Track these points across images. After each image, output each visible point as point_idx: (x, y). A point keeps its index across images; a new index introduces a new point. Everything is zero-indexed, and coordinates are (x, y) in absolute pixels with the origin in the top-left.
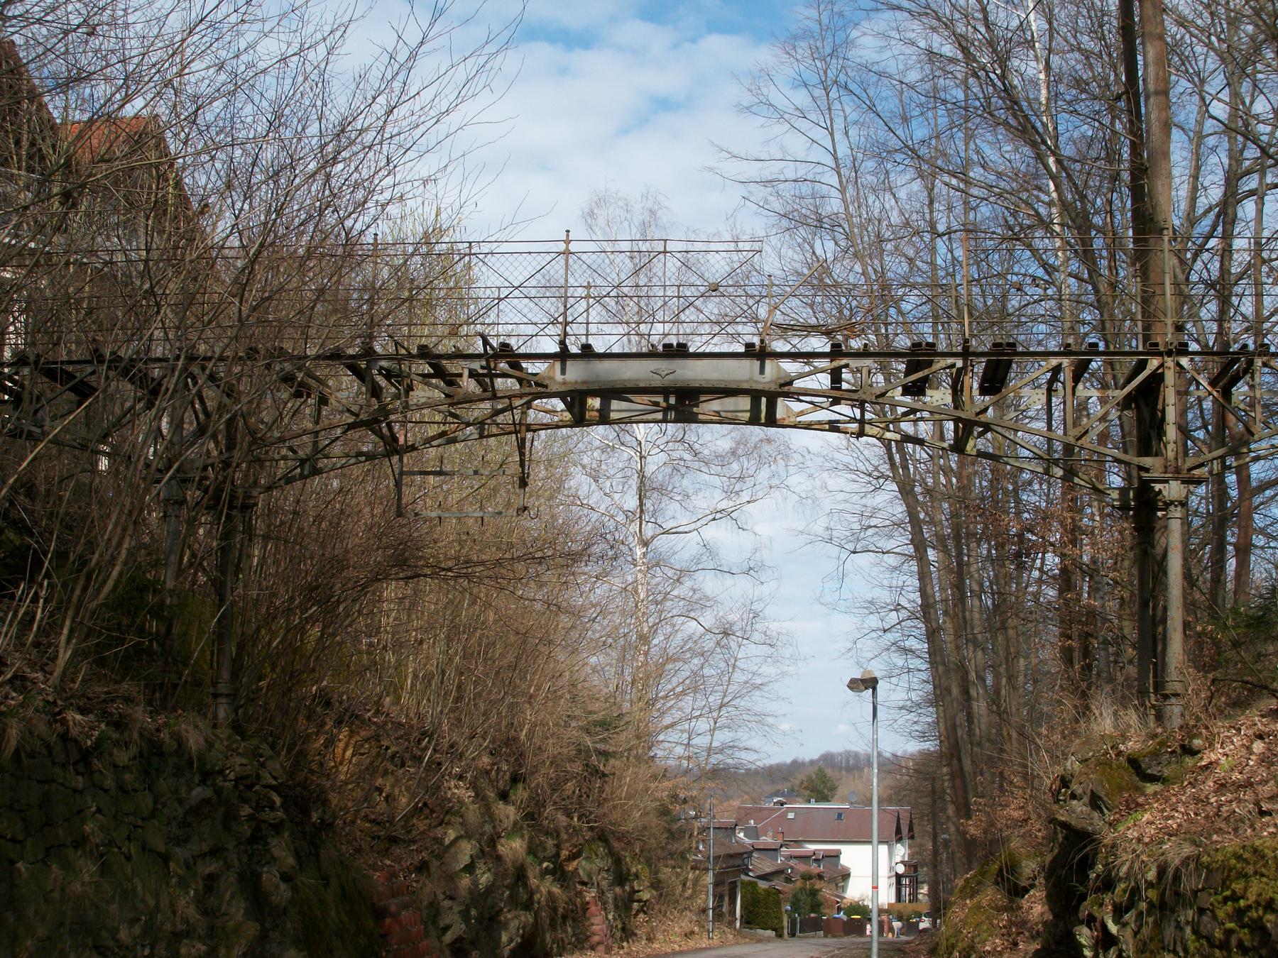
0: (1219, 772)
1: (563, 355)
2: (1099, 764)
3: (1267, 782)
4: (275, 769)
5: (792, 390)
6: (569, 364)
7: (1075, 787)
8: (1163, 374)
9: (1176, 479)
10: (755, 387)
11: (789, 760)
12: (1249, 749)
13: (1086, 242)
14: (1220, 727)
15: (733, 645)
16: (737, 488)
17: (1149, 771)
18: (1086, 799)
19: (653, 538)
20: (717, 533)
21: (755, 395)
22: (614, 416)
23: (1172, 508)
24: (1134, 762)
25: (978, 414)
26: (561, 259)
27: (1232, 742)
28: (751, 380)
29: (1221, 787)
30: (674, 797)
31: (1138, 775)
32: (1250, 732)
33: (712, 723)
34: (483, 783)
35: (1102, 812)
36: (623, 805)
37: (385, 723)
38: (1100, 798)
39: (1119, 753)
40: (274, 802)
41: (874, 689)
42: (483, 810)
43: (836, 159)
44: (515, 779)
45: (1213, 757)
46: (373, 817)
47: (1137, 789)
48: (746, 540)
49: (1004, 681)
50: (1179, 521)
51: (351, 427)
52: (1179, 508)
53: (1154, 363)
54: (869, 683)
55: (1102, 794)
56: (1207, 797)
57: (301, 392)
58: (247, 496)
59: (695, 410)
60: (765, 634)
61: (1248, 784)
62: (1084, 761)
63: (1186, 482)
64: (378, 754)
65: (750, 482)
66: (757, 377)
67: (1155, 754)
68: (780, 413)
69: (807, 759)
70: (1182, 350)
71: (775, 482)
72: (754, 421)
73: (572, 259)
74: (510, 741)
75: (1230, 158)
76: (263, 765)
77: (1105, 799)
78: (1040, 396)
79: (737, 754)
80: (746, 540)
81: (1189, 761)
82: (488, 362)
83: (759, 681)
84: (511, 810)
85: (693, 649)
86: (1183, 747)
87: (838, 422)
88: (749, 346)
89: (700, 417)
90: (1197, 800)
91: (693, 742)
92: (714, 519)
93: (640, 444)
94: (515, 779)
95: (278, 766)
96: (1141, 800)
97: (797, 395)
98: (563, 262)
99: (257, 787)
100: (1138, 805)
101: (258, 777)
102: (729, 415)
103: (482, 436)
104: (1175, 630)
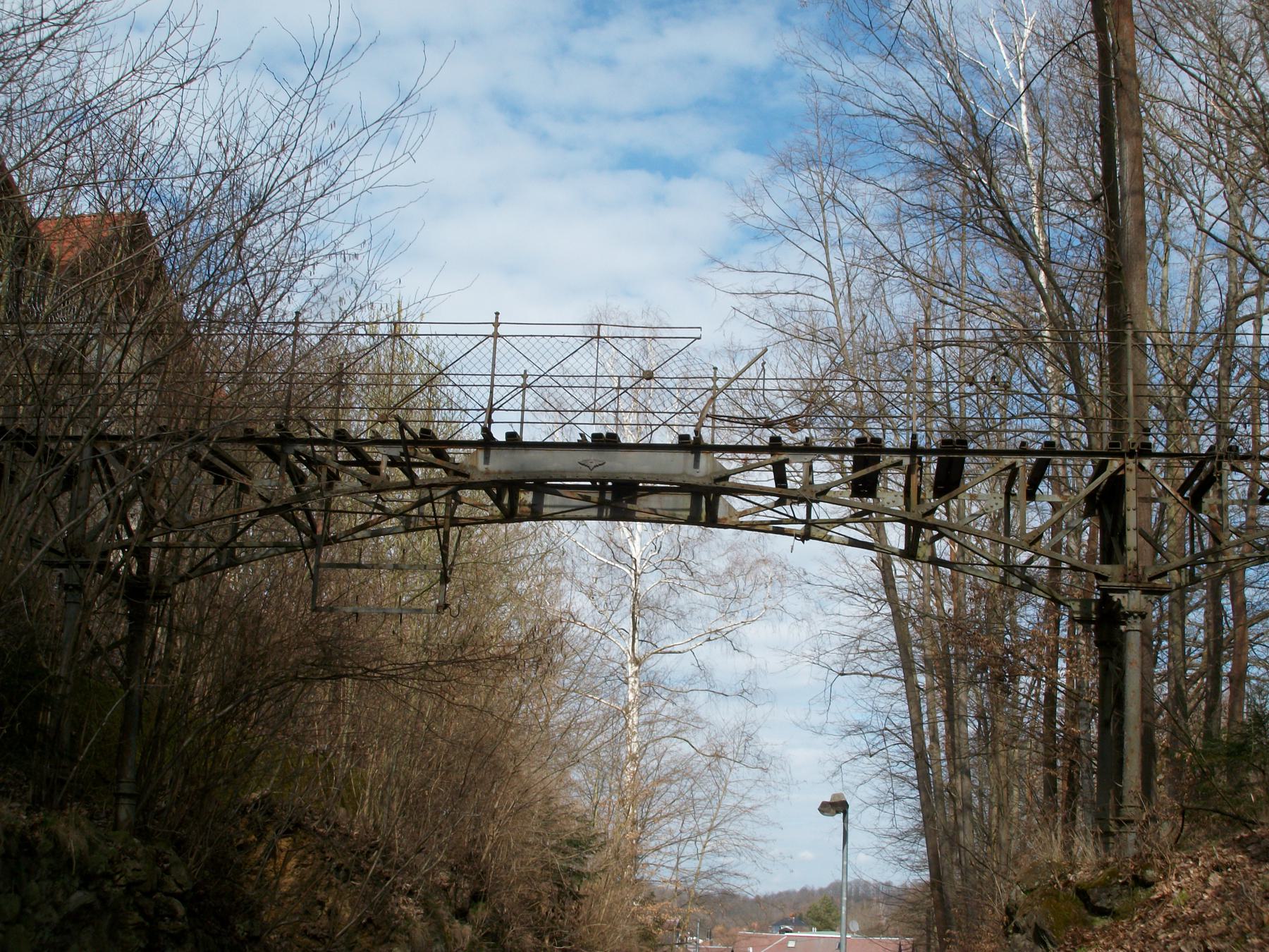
0: (1172, 907)
1: (487, 442)
2: (1045, 894)
3: (1219, 918)
4: (181, 875)
5: (727, 485)
6: (493, 452)
7: (1019, 920)
8: (1123, 476)
9: (1137, 589)
10: (693, 481)
11: (798, 888)
12: (1205, 881)
13: (1074, 362)
14: (1178, 860)
15: (725, 768)
16: (733, 608)
17: (1098, 904)
18: (1030, 933)
19: (646, 657)
20: (713, 653)
21: (695, 491)
22: (546, 511)
23: (1131, 619)
24: (1082, 893)
25: (925, 515)
26: (492, 339)
27: (1188, 874)
28: (684, 473)
29: (1171, 923)
30: (660, 923)
31: (1086, 907)
32: (1208, 864)
33: (700, 847)
34: (437, 900)
35: (1046, 946)
36: (600, 928)
37: (332, 835)
38: (1044, 932)
39: (1067, 883)
40: (175, 912)
41: (845, 813)
42: (433, 928)
43: (829, 272)
44: (476, 898)
45: (1166, 890)
46: (312, 931)
47: (1085, 923)
48: (741, 663)
49: (995, 809)
50: (1138, 634)
51: (263, 513)
52: (1139, 620)
53: (1115, 464)
54: (837, 807)
55: (1046, 927)
56: (1155, 934)
57: (220, 478)
58: (160, 586)
59: (629, 506)
60: (758, 757)
61: (1199, 920)
62: (1029, 891)
63: (1147, 592)
64: (322, 866)
65: (746, 602)
66: (691, 470)
67: (1105, 886)
68: (721, 513)
69: (816, 888)
70: (1146, 451)
71: (770, 603)
72: (693, 520)
73: (500, 342)
74: (470, 858)
75: (1230, 281)
76: (167, 871)
77: (1049, 933)
78: (998, 501)
79: (726, 880)
80: (741, 663)
81: (1141, 894)
82: (406, 449)
83: (748, 804)
84: (468, 929)
85: (682, 771)
86: (1135, 878)
87: (781, 522)
88: (683, 438)
89: (638, 515)
90: (1145, 937)
91: (681, 866)
92: (709, 640)
93: (635, 561)
94: (476, 898)
95: (183, 873)
96: (1087, 935)
97: (738, 491)
98: (491, 346)
99: (158, 895)
100: (1085, 941)
101: (161, 883)
102: (667, 513)
103: (407, 531)
104: (1132, 751)
